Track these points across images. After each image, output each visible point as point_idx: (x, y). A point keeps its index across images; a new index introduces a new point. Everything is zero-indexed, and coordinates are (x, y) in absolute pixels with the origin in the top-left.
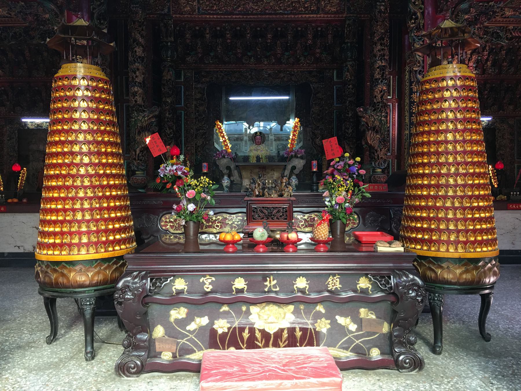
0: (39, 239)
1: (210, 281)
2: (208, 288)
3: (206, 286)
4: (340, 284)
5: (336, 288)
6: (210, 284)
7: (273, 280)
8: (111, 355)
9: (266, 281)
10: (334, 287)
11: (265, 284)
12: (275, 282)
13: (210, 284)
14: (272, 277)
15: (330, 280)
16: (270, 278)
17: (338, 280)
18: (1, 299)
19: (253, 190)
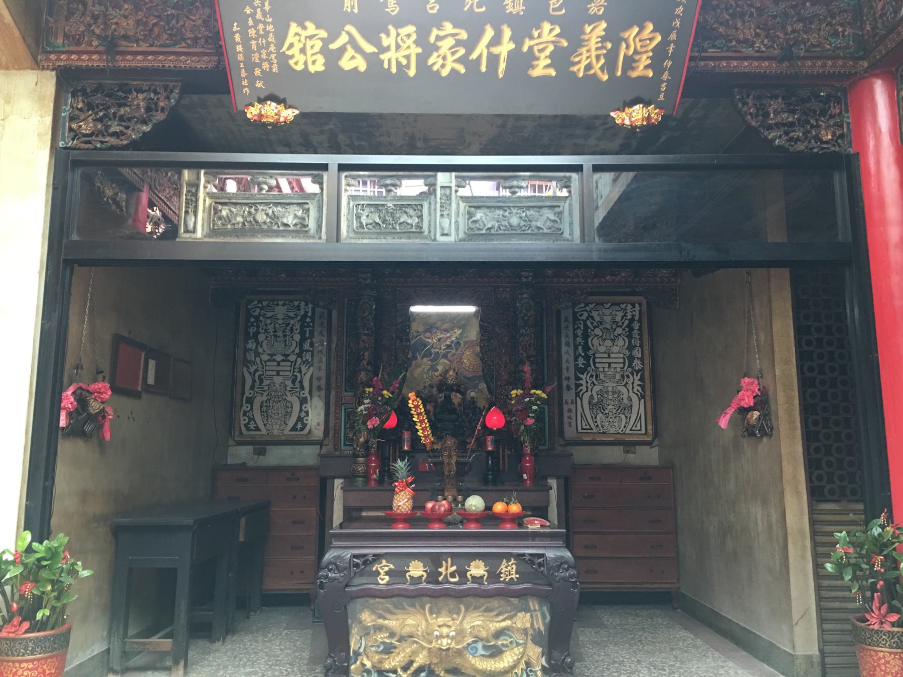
0: (513, 402)
1: (386, 569)
2: (382, 579)
3: (381, 576)
4: (516, 573)
5: (512, 578)
6: (387, 573)
7: (452, 566)
8: (258, 613)
9: (441, 566)
10: (509, 578)
11: (440, 570)
12: (454, 568)
13: (387, 573)
14: (449, 559)
15: (503, 566)
16: (447, 562)
17: (514, 566)
18: (11, 676)
19: (754, 43)
